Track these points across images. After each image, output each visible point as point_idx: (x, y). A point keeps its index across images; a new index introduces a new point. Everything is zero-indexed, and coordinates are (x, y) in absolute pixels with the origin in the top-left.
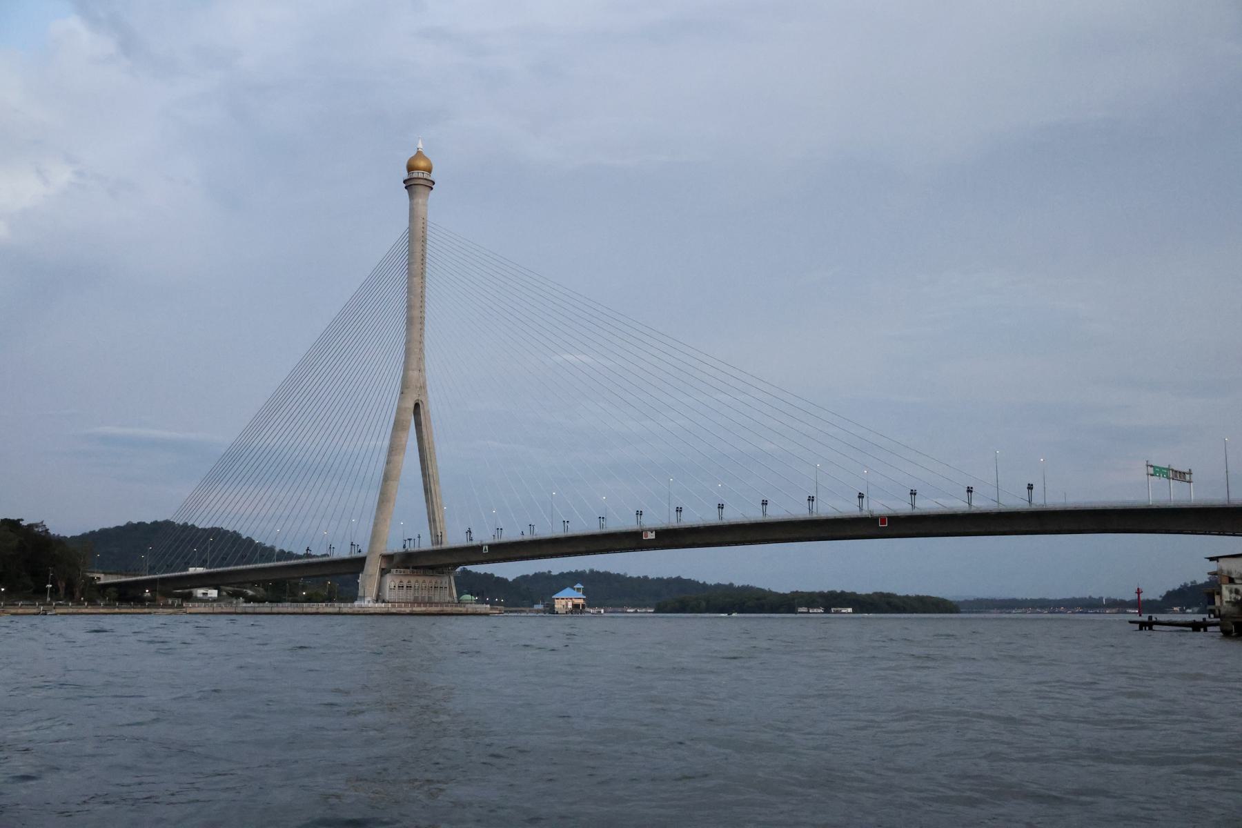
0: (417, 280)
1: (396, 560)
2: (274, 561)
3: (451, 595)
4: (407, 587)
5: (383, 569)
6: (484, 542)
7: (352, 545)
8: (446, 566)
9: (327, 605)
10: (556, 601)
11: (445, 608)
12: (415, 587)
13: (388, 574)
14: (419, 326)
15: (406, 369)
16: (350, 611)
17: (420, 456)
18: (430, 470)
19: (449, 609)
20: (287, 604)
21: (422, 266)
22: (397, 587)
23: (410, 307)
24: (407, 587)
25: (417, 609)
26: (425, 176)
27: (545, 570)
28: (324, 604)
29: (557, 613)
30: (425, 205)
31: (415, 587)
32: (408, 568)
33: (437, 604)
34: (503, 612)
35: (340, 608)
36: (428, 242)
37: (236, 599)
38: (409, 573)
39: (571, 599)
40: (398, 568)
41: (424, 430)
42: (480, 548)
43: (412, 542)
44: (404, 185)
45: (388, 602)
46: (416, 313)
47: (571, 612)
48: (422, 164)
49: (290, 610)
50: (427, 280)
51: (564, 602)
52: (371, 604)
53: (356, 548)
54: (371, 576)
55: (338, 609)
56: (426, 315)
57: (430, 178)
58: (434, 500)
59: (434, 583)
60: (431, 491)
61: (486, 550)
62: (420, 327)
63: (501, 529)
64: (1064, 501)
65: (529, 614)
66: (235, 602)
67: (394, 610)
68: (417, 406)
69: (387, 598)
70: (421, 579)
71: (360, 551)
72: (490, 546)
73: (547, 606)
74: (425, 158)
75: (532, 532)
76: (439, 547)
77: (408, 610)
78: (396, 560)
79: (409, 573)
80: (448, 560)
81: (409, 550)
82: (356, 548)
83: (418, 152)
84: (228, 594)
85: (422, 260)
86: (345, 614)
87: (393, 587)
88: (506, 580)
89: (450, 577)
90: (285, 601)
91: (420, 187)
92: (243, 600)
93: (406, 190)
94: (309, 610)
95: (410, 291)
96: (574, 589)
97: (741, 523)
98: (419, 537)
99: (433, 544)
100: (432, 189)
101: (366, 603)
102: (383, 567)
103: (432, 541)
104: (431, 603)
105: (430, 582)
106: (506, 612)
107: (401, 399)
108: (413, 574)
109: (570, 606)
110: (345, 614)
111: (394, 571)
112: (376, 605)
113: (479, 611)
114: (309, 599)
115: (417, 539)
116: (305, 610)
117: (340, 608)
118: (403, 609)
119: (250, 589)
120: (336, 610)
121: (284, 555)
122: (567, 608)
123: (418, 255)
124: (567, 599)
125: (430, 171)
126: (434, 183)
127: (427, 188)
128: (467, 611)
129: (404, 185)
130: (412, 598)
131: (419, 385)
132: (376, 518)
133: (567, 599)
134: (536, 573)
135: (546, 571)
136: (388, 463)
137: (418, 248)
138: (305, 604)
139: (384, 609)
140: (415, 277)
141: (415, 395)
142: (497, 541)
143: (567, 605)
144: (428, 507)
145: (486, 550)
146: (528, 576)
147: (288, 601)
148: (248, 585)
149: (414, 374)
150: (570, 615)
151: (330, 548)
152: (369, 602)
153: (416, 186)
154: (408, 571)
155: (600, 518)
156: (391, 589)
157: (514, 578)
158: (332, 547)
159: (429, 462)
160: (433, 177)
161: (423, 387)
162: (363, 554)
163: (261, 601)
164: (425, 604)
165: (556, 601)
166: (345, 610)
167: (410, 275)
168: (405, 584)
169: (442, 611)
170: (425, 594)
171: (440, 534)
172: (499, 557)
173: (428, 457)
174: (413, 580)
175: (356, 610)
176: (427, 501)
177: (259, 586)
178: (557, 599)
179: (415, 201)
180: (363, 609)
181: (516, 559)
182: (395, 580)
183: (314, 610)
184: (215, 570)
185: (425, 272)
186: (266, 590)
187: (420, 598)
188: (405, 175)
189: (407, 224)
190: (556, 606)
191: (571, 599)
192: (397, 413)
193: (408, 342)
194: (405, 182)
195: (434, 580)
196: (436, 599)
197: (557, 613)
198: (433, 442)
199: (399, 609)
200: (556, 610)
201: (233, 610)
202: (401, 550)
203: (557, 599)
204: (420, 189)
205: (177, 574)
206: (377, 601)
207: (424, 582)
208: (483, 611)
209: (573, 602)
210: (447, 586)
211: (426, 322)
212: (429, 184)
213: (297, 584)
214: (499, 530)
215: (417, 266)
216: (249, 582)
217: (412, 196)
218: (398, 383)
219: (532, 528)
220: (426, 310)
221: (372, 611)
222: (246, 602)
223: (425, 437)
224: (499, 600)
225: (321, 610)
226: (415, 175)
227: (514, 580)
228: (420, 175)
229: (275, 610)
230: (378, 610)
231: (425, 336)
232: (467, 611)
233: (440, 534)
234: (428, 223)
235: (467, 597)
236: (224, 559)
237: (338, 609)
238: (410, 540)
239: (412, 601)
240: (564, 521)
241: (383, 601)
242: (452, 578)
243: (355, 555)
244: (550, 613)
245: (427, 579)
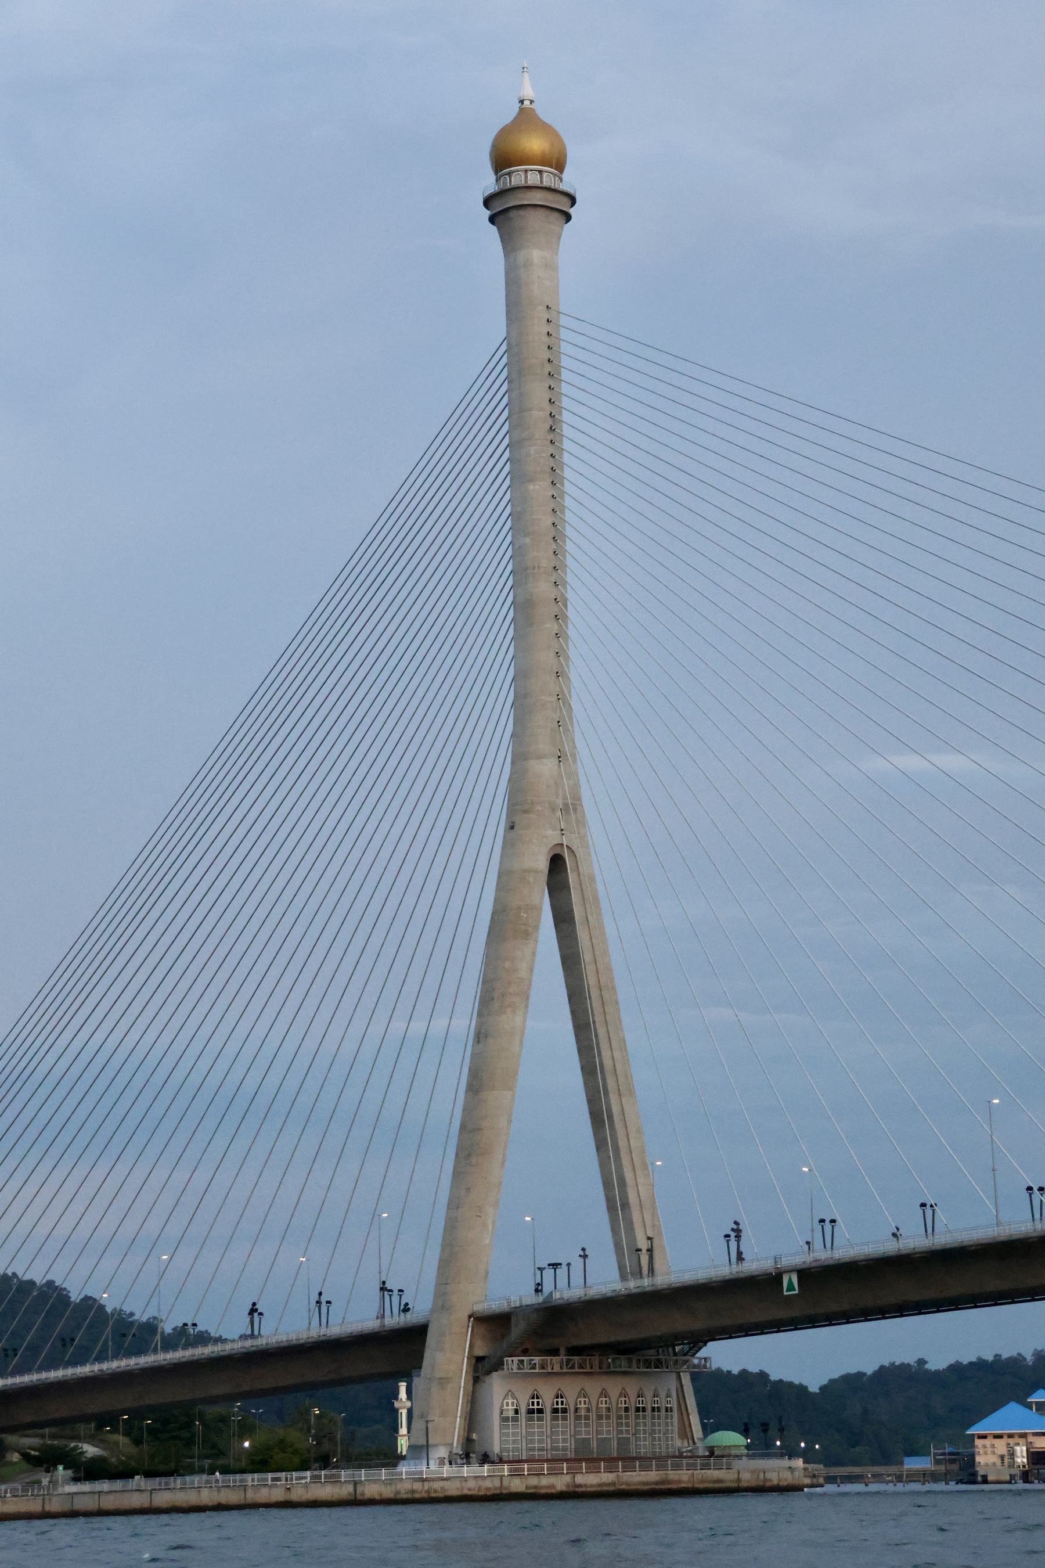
0: (539, 489)
1: (517, 1330)
2: (155, 1351)
3: (685, 1432)
4: (555, 1411)
5: (479, 1359)
6: (785, 1262)
7: (383, 1289)
8: (668, 1341)
9: (316, 1479)
10: (978, 1442)
11: (673, 1475)
12: (576, 1410)
13: (495, 1374)
14: (553, 627)
15: (520, 757)
16: (388, 1492)
17: (573, 1012)
18: (606, 1054)
19: (683, 1477)
20: (196, 1479)
21: (551, 450)
22: (523, 1410)
23: (521, 573)
24: (555, 1411)
25: (588, 1480)
26: (548, 181)
27: (908, 1357)
28: (308, 1473)
29: (985, 1481)
30: (551, 267)
31: (576, 1410)
32: (555, 1352)
33: (645, 1462)
34: (821, 1480)
35: (355, 1483)
36: (565, 375)
37: (48, 1471)
38: (557, 1369)
39: (1023, 1436)
40: (525, 1352)
41: (582, 935)
42: (771, 1281)
43: (562, 1272)
44: (487, 213)
45: (501, 1461)
46: (543, 588)
47: (1026, 1477)
48: (535, 144)
49: (207, 1497)
50: (568, 487)
51: (1001, 1446)
52: (446, 1470)
53: (395, 1299)
54: (443, 1381)
55: (350, 1488)
56: (570, 595)
57: (563, 187)
58: (622, 1143)
59: (633, 1398)
60: (610, 1117)
61: (791, 1287)
62: (555, 628)
63: (833, 1221)
64: (41, 1509)
65: (873, 1487)
66: (45, 1481)
67: (517, 1485)
68: (557, 863)
69: (496, 1449)
70: (593, 1387)
71: (406, 1309)
72: (805, 1274)
73: (953, 1458)
74: (546, 129)
75: (929, 1228)
76: (646, 1283)
77: (561, 1483)
78: (517, 1330)
79: (557, 1369)
80: (680, 1322)
81: (557, 1295)
82: (395, 1299)
83: (522, 110)
84: (26, 1457)
85: (552, 429)
86: (371, 1502)
87: (511, 1414)
88: (802, 1389)
89: (679, 1378)
90: (191, 1471)
91: (532, 215)
92: (70, 1473)
93: (494, 229)
94: (264, 1495)
95: (519, 520)
96: (1029, 1406)
97: (955, 1245)
98: (585, 1257)
99: (623, 1277)
100: (568, 217)
101: (433, 1466)
102: (479, 1352)
103: (621, 1268)
104: (629, 1461)
105: (624, 1394)
106: (831, 1480)
107: (509, 846)
108: (569, 1372)
109: (1021, 1457)
110: (371, 1502)
111: (512, 1363)
112: (466, 1471)
113: (774, 1478)
114: (260, 1463)
115: (577, 1264)
116: (251, 1496)
117: (355, 1483)
118: (545, 1481)
119: (91, 1439)
120: (345, 1491)
121: (183, 1336)
122: (1012, 1464)
123: (538, 415)
124: (1010, 1436)
125: (559, 165)
126: (573, 201)
127: (556, 215)
128: (739, 1480)
129: (487, 213)
130: (571, 1445)
131: (560, 803)
132: (454, 1204)
133: (1010, 1436)
134: (882, 1367)
135: (910, 1359)
136: (481, 1036)
137: (537, 392)
138: (249, 1477)
139: (488, 1484)
140: (532, 480)
141: (550, 832)
142: (822, 1255)
143: (1012, 1454)
144: (604, 1165)
145: (791, 1287)
146: (860, 1375)
147: (202, 1471)
148: (82, 1428)
149: (545, 769)
150: (1021, 1485)
151: (318, 1302)
152: (441, 1462)
153: (522, 212)
154: (555, 1362)
155: (923, 1205)
156: (505, 1419)
157: (824, 1381)
158: (324, 1299)
159: (601, 1032)
160: (569, 181)
161: (571, 807)
162: (421, 1309)
163: (125, 1474)
164: (611, 1462)
165: (978, 1442)
166: (370, 1491)
167: (519, 477)
168: (548, 1400)
169: (662, 1482)
170: (609, 1431)
171: (643, 1244)
172: (833, 1307)
173: (599, 1019)
174: (572, 1389)
175: (404, 1488)
176: (600, 1145)
177: (115, 1430)
178: (984, 1437)
179: (521, 256)
180: (427, 1485)
181: (883, 1312)
182: (588, 1390)
183: (278, 1494)
184: (44, 1375)
185: (561, 464)
186: (137, 1442)
187: (615, 1444)
188: (489, 183)
189: (499, 328)
190: (978, 1459)
191: (1023, 1436)
192: (501, 887)
193: (522, 677)
194: (487, 202)
195: (631, 1386)
196: (643, 1446)
197: (985, 1481)
198: (610, 970)
199: (533, 1481)
200: (981, 1472)
201: (35, 1506)
202: (530, 1298)
203: (984, 1437)
204: (534, 220)
205: (26, 1379)
206: (466, 1457)
207: (604, 1394)
208: (787, 1478)
209: (1029, 1445)
210: (674, 1405)
211: (571, 612)
212: (563, 204)
213: (224, 1420)
214: (828, 1227)
215: (536, 451)
216: (86, 1419)
217: (509, 242)
218: (499, 800)
219: (929, 1212)
220: (570, 578)
221: (453, 1489)
222: (76, 1480)
223: (586, 956)
224: (810, 1448)
225: (298, 1494)
226: (517, 179)
227: (823, 1388)
228: (533, 179)
229: (163, 1499)
230: (471, 1487)
231: (572, 652)
232: (739, 1480)
233: (643, 1244)
234: (563, 320)
235: (730, 1439)
236: (34, 1349)
237: (350, 1488)
238: (555, 1266)
239: (570, 1455)
240: (1030, 1189)
241: (485, 1459)
242: (686, 1380)
243: (394, 1320)
244: (960, 1482)
245: (614, 1386)
